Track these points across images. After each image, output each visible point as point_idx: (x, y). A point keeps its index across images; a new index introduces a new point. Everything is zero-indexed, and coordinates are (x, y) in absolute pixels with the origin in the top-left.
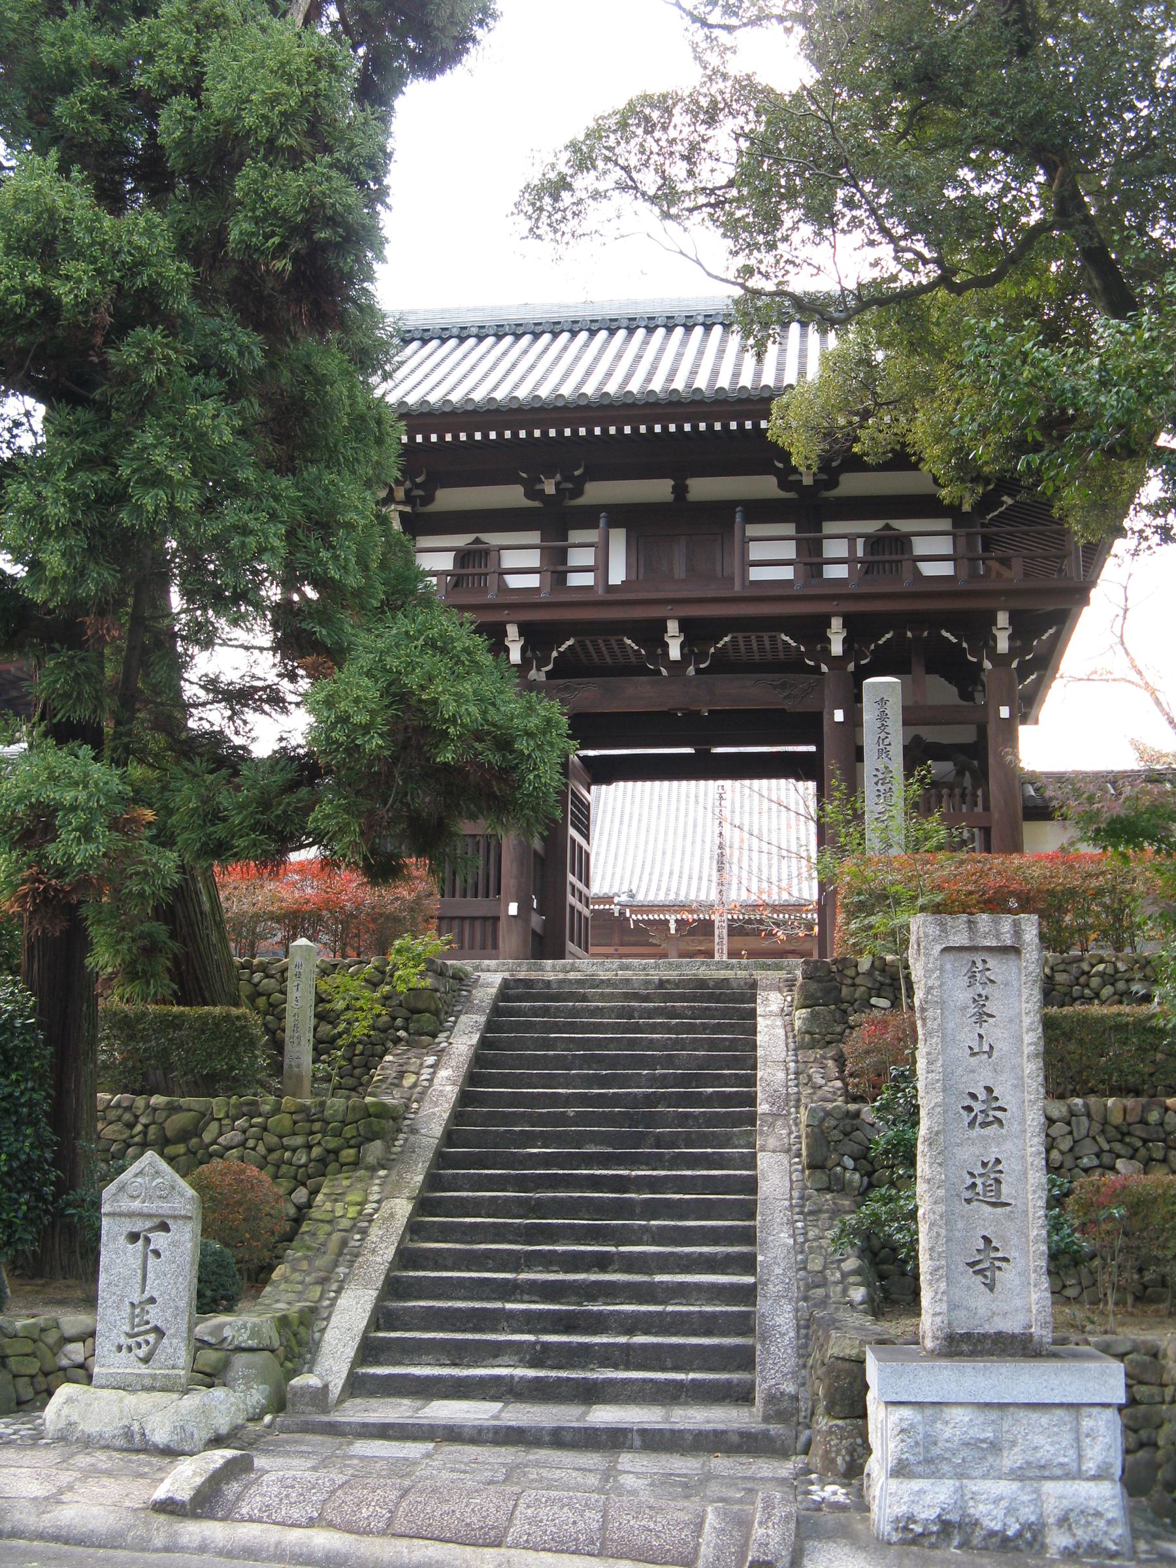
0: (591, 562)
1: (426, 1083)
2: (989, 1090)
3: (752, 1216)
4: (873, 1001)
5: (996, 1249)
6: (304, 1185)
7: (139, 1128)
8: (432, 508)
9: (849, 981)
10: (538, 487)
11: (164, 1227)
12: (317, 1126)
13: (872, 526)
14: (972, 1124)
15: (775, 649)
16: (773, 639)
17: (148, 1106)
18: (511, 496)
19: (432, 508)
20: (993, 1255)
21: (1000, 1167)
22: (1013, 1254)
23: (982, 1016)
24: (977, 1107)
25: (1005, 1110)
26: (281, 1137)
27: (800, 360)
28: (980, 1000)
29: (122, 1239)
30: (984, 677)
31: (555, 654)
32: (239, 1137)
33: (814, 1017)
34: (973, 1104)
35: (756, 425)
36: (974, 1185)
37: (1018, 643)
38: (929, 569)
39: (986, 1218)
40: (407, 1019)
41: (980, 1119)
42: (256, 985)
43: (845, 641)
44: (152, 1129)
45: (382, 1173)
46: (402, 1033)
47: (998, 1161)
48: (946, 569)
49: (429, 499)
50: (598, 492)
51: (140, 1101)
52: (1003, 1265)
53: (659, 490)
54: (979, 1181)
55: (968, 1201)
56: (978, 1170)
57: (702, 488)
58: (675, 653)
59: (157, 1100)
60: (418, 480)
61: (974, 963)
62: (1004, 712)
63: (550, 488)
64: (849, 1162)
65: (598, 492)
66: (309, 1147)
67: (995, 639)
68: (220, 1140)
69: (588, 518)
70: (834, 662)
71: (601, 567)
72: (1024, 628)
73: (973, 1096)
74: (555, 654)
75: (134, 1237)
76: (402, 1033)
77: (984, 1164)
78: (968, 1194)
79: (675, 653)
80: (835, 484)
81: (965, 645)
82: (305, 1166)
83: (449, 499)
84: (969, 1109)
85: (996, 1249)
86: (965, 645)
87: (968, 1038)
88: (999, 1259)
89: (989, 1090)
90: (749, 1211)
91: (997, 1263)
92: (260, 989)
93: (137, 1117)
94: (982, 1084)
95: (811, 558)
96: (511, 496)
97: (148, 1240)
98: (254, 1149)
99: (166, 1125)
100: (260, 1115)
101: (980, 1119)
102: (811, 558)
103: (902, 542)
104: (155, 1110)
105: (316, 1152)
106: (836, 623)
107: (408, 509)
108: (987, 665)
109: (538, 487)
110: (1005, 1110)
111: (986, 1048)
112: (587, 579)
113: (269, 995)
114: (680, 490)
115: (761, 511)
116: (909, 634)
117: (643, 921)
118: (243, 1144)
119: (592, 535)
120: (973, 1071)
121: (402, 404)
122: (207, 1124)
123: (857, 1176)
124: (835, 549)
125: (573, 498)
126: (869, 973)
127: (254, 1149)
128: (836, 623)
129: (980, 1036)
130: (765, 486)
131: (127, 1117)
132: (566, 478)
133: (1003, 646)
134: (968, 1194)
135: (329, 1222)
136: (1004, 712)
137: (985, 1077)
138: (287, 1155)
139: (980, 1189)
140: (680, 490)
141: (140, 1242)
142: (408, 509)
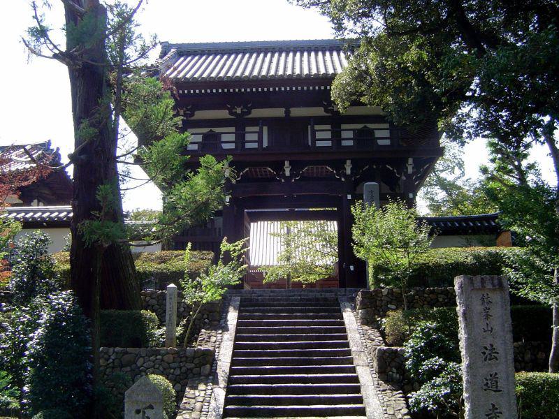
0: (256, 139)
1: (220, 341)
2: (492, 345)
3: (359, 391)
4: (389, 306)
5: (497, 409)
6: (179, 383)
7: (111, 360)
8: (194, 118)
9: (379, 299)
10: (234, 111)
11: (151, 407)
12: (183, 359)
13: (206, 130)
14: (485, 360)
15: (266, 174)
16: (265, 170)
17: (114, 351)
18: (223, 114)
19: (194, 118)
20: (496, 411)
21: (497, 376)
22: (504, 410)
23: (488, 316)
24: (487, 352)
25: (498, 353)
26: (169, 364)
27: (338, 65)
28: (487, 310)
29: (134, 412)
30: (400, 182)
31: (241, 173)
32: (152, 364)
33: (367, 312)
34: (485, 351)
35: (326, 88)
36: (487, 383)
37: (415, 170)
38: (381, 142)
39: (493, 398)
40: (208, 315)
41: (488, 357)
42: (147, 302)
43: (351, 169)
44: (117, 361)
45: (211, 377)
46: (206, 320)
47: (496, 374)
48: (387, 142)
49: (192, 115)
50: (257, 113)
51: (111, 350)
52: (500, 415)
53: (279, 112)
54: (489, 382)
55: (485, 390)
56: (489, 378)
57: (296, 112)
58: (287, 173)
59: (118, 349)
60: (189, 108)
61: (483, 295)
62: (349, 197)
63: (239, 111)
64: (394, 370)
65: (257, 113)
66: (181, 368)
67: (407, 168)
68: (145, 365)
69: (255, 122)
70: (286, 178)
71: (260, 141)
72: (417, 165)
73: (486, 348)
74: (241, 173)
75: (138, 412)
76: (206, 320)
77: (491, 375)
78: (485, 387)
79: (287, 173)
80: (250, 113)
81: (395, 171)
82: (179, 375)
83: (200, 115)
84: (484, 353)
85: (497, 409)
86: (395, 171)
87: (482, 325)
88: (498, 413)
89: (492, 345)
90: (358, 390)
91: (497, 414)
92: (149, 303)
93: (110, 356)
94: (489, 343)
95: (336, 137)
96: (223, 114)
97: (144, 413)
98: (158, 369)
99: (122, 359)
100: (160, 355)
101: (488, 357)
102: (336, 137)
103: (371, 132)
104: (117, 353)
105: (184, 369)
106: (348, 162)
107: (185, 118)
108: (404, 178)
109: (234, 111)
110: (498, 353)
111: (490, 329)
112: (255, 145)
113: (153, 306)
114: (287, 112)
115: (320, 120)
116: (375, 167)
117: (254, 273)
118: (154, 367)
119: (257, 129)
120: (485, 338)
121: (176, 77)
122: (139, 358)
123: (398, 376)
124: (344, 135)
125: (190, 117)
126: (386, 296)
127: (158, 369)
128: (348, 162)
129: (487, 324)
130: (319, 111)
131: (106, 356)
132: (245, 107)
133: (410, 170)
134: (485, 387)
135: (194, 398)
136: (349, 197)
137: (489, 340)
138: (172, 370)
139: (490, 385)
140: (287, 112)
141: (141, 413)
142: (185, 118)
